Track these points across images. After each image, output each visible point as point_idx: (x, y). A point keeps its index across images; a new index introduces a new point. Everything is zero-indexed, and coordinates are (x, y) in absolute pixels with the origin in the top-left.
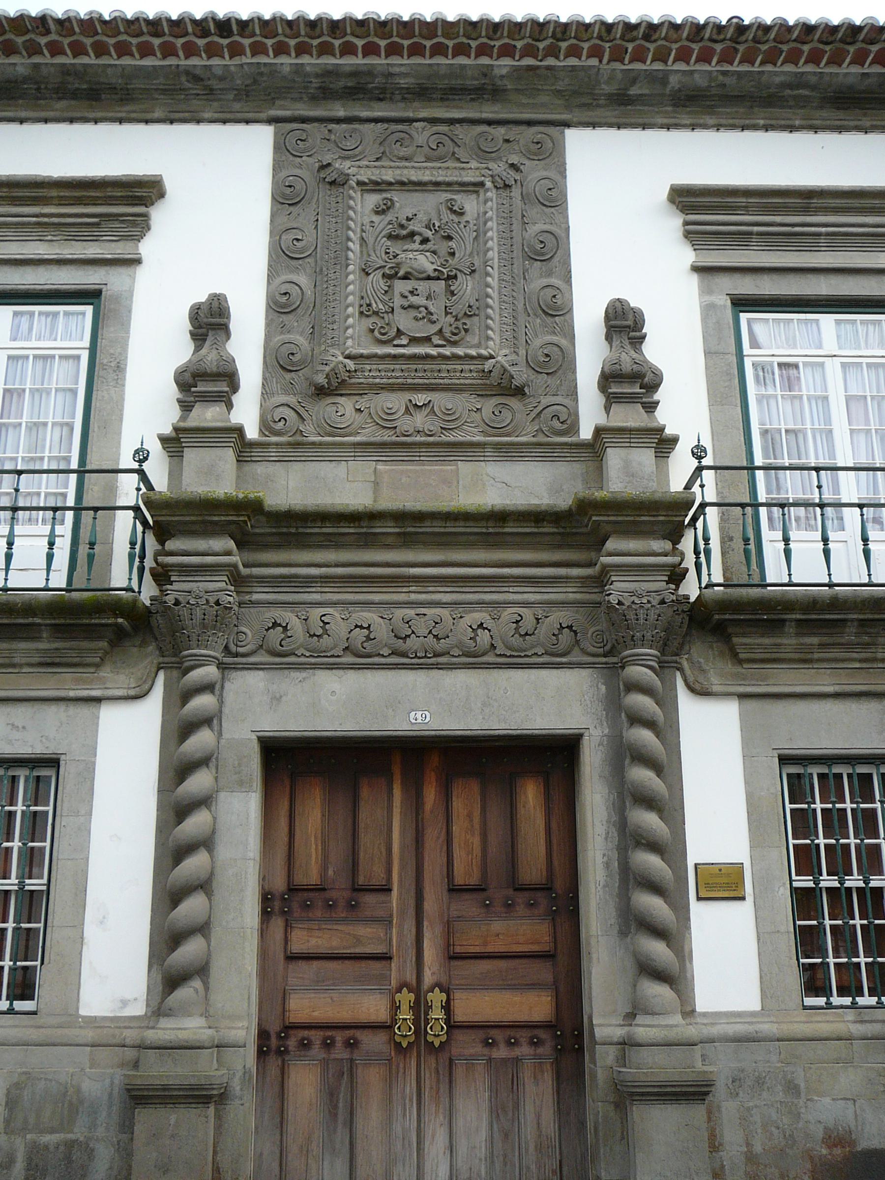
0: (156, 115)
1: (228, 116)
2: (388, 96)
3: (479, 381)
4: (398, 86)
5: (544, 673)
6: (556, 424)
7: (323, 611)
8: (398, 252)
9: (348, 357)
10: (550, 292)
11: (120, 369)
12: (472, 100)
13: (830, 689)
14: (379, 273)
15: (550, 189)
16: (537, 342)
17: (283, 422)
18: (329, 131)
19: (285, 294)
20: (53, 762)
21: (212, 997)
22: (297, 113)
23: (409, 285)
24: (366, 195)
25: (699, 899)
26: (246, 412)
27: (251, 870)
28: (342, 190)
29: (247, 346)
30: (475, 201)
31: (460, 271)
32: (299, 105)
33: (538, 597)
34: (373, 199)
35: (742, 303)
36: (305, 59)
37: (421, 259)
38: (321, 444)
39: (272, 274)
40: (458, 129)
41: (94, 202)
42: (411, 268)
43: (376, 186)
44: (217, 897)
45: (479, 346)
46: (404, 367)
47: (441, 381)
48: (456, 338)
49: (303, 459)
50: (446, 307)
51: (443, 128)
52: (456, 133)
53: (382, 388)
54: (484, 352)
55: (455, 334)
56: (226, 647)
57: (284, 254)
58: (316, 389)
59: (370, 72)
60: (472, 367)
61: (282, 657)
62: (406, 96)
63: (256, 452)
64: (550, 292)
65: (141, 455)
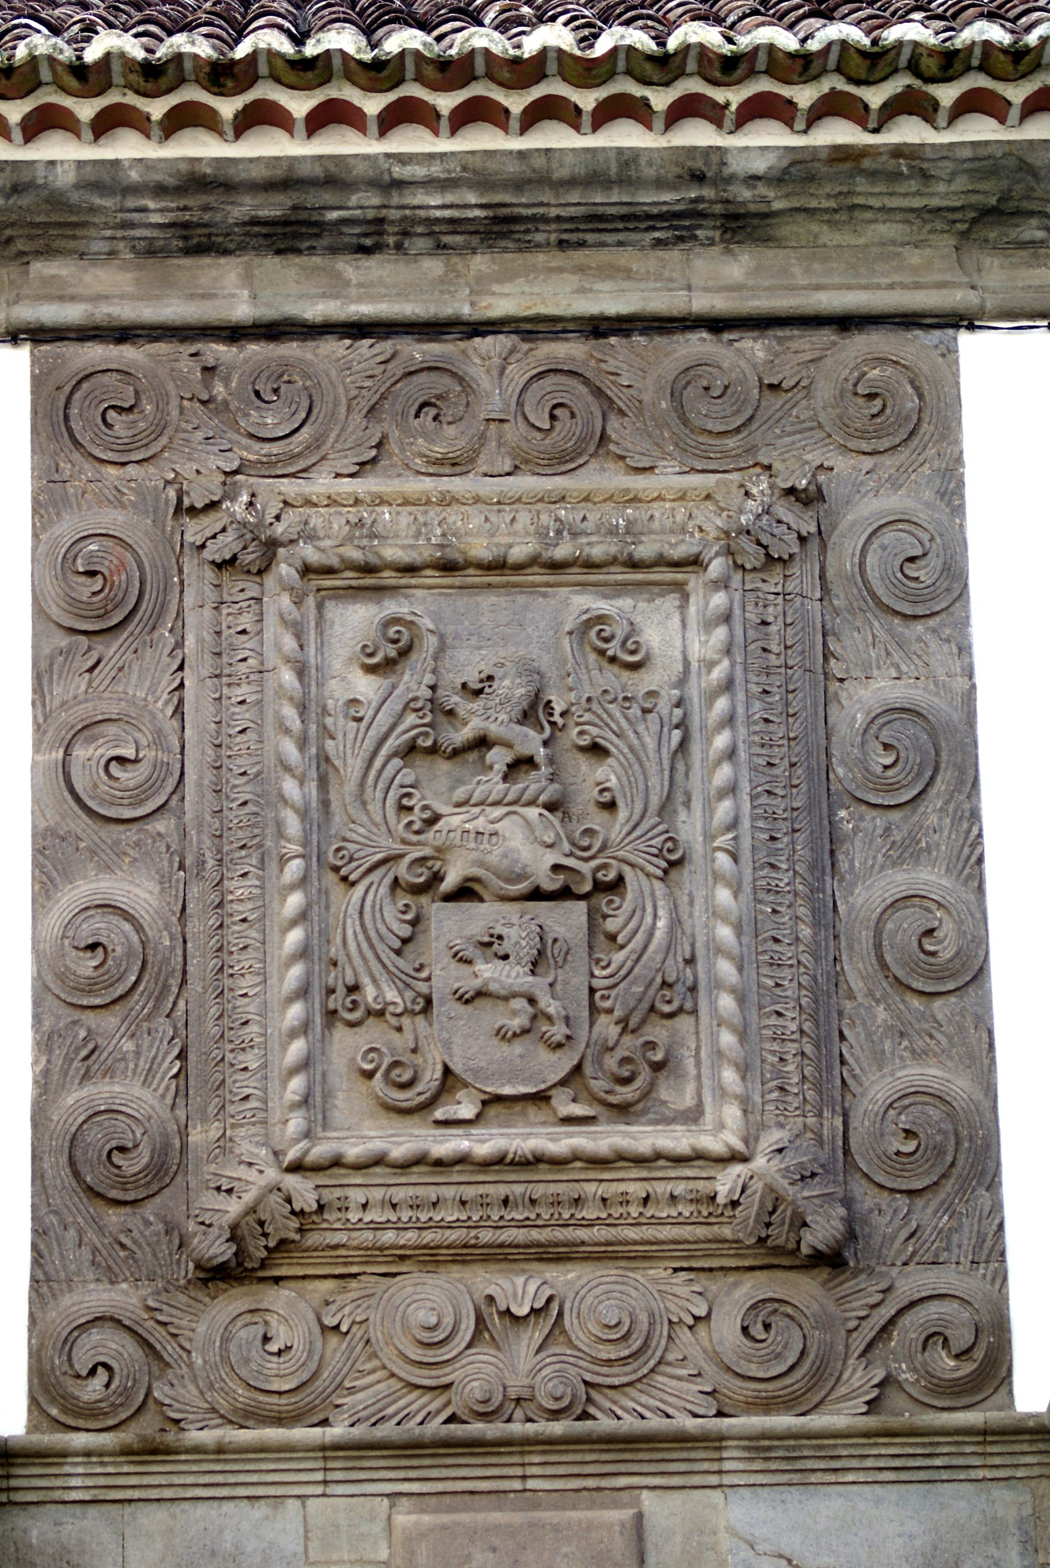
2: (391, 240)
3: (700, 1232)
4: (422, 213)
6: (946, 1364)
8: (443, 809)
9: (297, 1168)
10: (911, 921)
12: (658, 243)
14: (381, 879)
15: (912, 559)
17: (102, 1375)
18: (209, 370)
19: (93, 947)
24: (335, 611)
28: (253, 591)
30: (676, 621)
31: (632, 865)
39: (53, 860)
40: (620, 355)
42: (482, 864)
46: (470, 1192)
47: (582, 1234)
48: (626, 1093)
49: (168, 1493)
50: (592, 991)
51: (570, 350)
52: (612, 365)
53: (402, 1258)
54: (712, 1144)
55: (626, 1081)
58: (198, 1267)
59: (334, 177)
60: (680, 1188)
62: (446, 239)
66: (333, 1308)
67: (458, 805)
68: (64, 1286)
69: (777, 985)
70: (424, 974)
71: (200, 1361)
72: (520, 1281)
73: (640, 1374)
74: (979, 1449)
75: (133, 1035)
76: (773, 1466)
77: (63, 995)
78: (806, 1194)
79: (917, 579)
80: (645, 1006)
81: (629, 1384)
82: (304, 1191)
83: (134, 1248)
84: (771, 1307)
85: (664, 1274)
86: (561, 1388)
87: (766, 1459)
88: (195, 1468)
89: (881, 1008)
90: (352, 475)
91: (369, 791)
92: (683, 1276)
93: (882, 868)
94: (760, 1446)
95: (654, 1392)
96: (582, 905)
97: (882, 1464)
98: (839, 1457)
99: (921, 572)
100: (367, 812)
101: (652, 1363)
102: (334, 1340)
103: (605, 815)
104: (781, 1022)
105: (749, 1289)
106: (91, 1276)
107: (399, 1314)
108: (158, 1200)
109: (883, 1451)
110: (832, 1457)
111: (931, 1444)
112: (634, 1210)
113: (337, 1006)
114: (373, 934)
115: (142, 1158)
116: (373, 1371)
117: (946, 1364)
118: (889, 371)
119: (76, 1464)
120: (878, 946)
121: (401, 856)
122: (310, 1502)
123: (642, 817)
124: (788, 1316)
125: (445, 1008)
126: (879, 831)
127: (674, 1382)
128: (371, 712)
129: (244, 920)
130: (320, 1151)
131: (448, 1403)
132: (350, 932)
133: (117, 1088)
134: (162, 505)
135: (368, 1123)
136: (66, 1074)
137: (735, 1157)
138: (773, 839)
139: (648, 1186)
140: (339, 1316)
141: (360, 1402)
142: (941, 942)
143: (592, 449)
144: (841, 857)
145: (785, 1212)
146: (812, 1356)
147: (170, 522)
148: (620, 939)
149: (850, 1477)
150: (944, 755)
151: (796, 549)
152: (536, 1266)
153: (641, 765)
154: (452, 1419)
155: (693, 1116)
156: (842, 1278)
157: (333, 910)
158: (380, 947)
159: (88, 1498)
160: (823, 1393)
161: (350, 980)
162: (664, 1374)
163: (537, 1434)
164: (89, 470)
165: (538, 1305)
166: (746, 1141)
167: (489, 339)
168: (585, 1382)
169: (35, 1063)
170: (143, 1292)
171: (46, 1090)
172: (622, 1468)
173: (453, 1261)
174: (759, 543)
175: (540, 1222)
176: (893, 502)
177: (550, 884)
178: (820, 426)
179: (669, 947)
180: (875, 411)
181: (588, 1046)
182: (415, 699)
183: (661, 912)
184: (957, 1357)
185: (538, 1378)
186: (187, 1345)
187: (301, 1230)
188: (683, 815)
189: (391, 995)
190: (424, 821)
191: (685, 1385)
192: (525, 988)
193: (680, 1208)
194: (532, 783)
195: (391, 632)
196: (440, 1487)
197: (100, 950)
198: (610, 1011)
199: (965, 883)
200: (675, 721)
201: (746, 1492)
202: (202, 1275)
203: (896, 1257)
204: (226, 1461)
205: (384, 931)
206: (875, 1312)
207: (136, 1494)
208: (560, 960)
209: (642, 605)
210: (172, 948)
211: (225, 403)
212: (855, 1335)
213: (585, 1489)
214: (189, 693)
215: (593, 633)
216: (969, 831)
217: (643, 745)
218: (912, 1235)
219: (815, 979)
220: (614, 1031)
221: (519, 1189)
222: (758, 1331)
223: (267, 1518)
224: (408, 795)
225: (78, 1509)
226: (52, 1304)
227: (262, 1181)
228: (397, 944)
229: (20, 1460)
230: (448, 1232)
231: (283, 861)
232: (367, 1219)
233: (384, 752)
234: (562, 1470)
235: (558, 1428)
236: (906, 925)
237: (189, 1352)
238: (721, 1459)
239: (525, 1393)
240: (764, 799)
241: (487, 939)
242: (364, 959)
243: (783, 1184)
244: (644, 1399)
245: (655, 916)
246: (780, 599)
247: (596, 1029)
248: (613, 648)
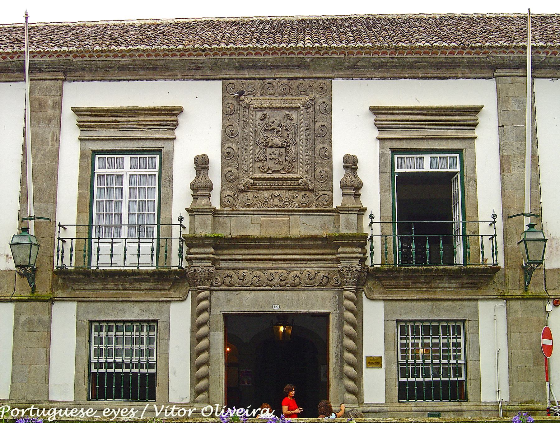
0: (178, 77)
1: (205, 77)
5: (318, 292)
6: (325, 202)
7: (244, 271)
11: (171, 181)
13: (415, 298)
16: (319, 170)
20: (156, 322)
21: (210, 397)
22: (231, 76)
23: (272, 150)
25: (367, 367)
26: (216, 202)
27: (221, 357)
29: (215, 175)
32: (230, 72)
33: (316, 265)
34: (259, 114)
35: (394, 152)
36: (233, 57)
37: (277, 139)
38: (242, 211)
39: (223, 143)
40: (292, 82)
41: (158, 115)
43: (261, 109)
44: (211, 366)
45: (297, 173)
48: (289, 170)
54: (299, 177)
56: (211, 284)
57: (227, 136)
61: (231, 287)
63: (220, 213)
64: (323, 150)
65: (181, 219)
105: (303, 193)
113: (257, 160)
130: (254, 177)
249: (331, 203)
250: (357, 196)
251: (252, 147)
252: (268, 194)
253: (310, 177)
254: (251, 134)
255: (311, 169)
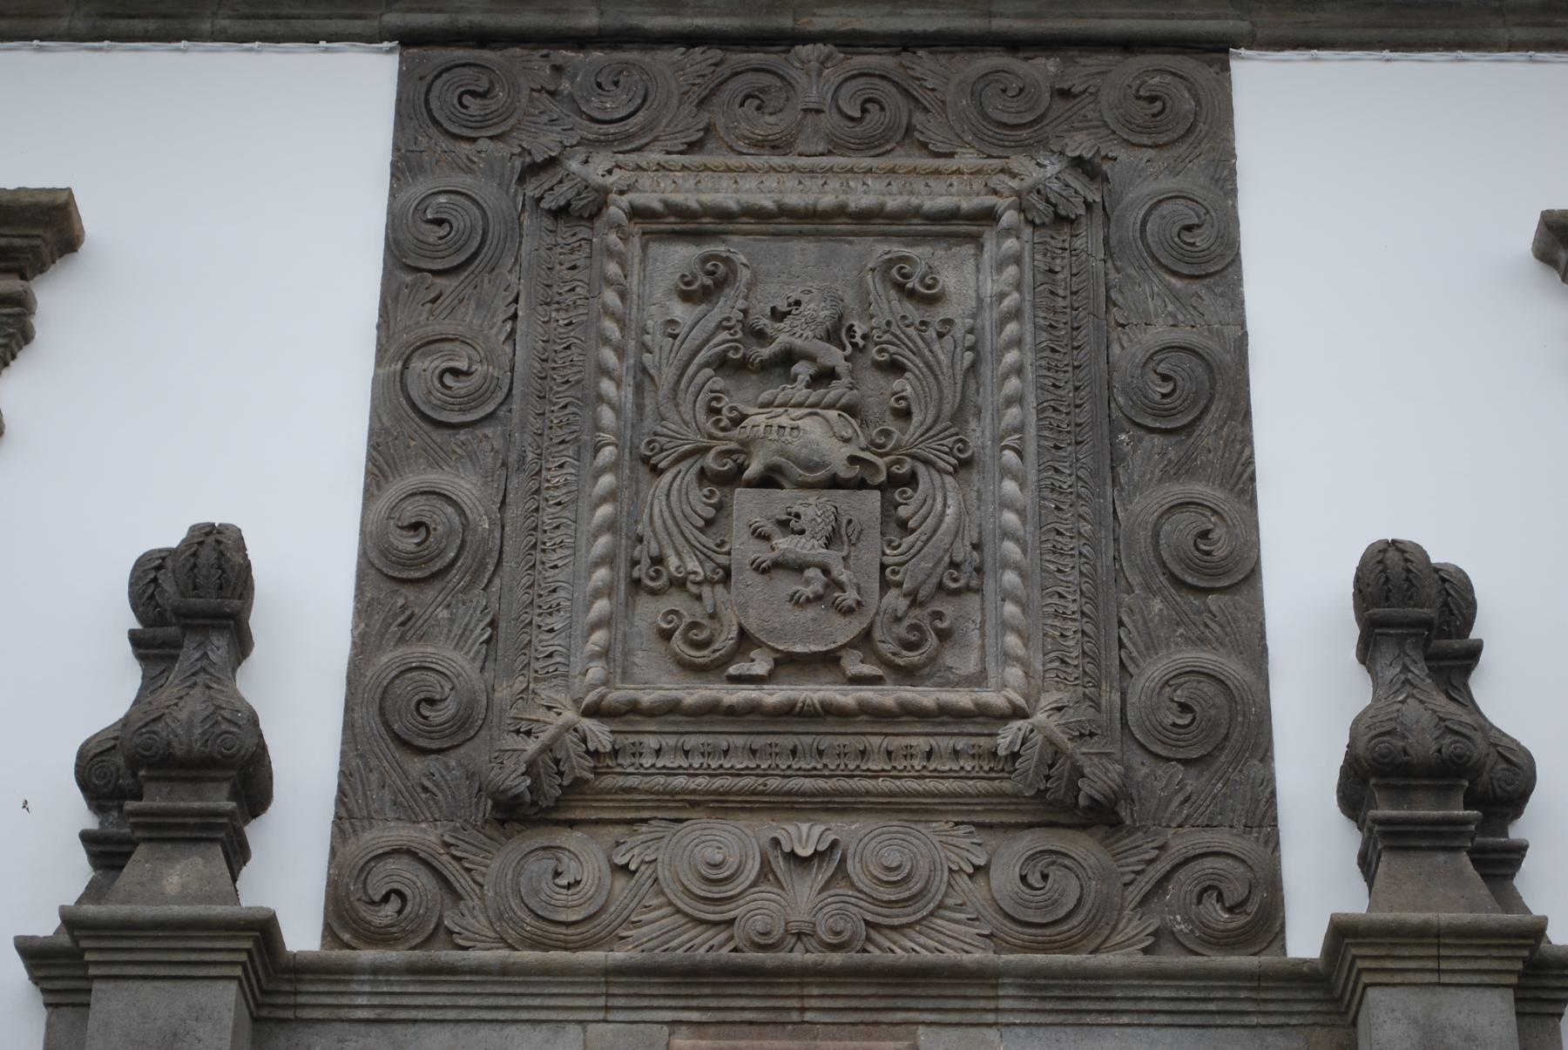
3: (982, 785)
6: (1219, 916)
8: (751, 410)
9: (594, 711)
14: (689, 470)
15: (1189, 228)
16: (1153, 671)
18: (557, 69)
23: (782, 499)
24: (656, 249)
29: (299, 684)
30: (971, 265)
34: (682, 256)
39: (383, 461)
40: (925, 63)
43: (686, 224)
46: (759, 742)
47: (868, 784)
48: (913, 657)
49: (451, 1015)
50: (883, 567)
52: (918, 72)
54: (993, 698)
57: (416, 416)
60: (961, 743)
66: (623, 848)
67: (763, 406)
68: (366, 823)
69: (1059, 571)
70: (725, 549)
71: (491, 894)
72: (805, 827)
73: (919, 915)
74: (1253, 995)
75: (448, 606)
76: (1050, 1006)
77: (385, 570)
78: (1084, 750)
79: (1193, 244)
80: (934, 580)
81: (909, 925)
82: (600, 734)
83: (435, 790)
84: (1048, 859)
85: (946, 827)
86: (842, 923)
87: (1043, 998)
88: (479, 990)
89: (1158, 600)
90: (681, 153)
91: (681, 394)
92: (963, 829)
93: (1160, 480)
94: (1036, 983)
95: (933, 933)
96: (877, 494)
97: (1156, 1006)
98: (1113, 999)
99: (1200, 240)
100: (679, 413)
101: (931, 906)
102: (621, 882)
103: (901, 424)
104: (1062, 602)
105: (1028, 842)
106: (390, 815)
107: (687, 853)
108: (462, 750)
109: (1157, 994)
110: (1107, 999)
111: (1205, 988)
112: (917, 764)
113: (642, 579)
114: (678, 513)
115: (447, 710)
116: (660, 907)
117: (1219, 916)
118: (1168, 79)
119: (363, 982)
120: (1156, 544)
121: (709, 449)
122: (590, 1027)
123: (935, 422)
124: (1066, 867)
125: (744, 578)
126: (1157, 450)
127: (953, 926)
128: (686, 329)
129: (559, 504)
130: (618, 695)
131: (731, 938)
132: (656, 511)
133: (429, 650)
134: (507, 173)
135: (664, 679)
136: (383, 636)
137: (1018, 713)
138: (1057, 447)
139: (932, 741)
140: (628, 856)
141: (644, 935)
142: (1215, 543)
143: (898, 137)
144: (1120, 470)
145: (1063, 767)
146: (1088, 905)
147: (513, 186)
148: (911, 524)
149: (1125, 1019)
150: (1218, 386)
151: (1082, 211)
152: (824, 816)
153: (936, 377)
154: (735, 950)
155: (978, 680)
156: (1119, 835)
157: (642, 495)
158: (684, 524)
159: (372, 1016)
160: (1099, 940)
161: (654, 550)
162: (942, 918)
163: (816, 964)
164: (445, 143)
165: (821, 848)
166: (1026, 697)
167: (810, 47)
168: (867, 923)
169: (355, 627)
170: (439, 831)
171: (363, 649)
172: (899, 1003)
173: (742, 809)
174: (1048, 201)
175: (826, 773)
176: (1169, 184)
177: (845, 472)
178: (1106, 125)
179: (957, 533)
180: (1155, 111)
181: (877, 613)
182: (728, 319)
183: (950, 502)
184: (1230, 910)
185: (820, 915)
186: (480, 880)
187: (594, 770)
188: (973, 424)
189: (693, 565)
190: (731, 420)
191: (963, 928)
192: (819, 558)
193: (962, 763)
194: (835, 391)
195: (709, 266)
196: (720, 1016)
197: (423, 531)
198: (899, 585)
199: (1238, 496)
200: (967, 344)
201: (1022, 1031)
202: (498, 816)
203: (1171, 820)
204: (509, 983)
205: (688, 511)
206: (1150, 868)
207: (421, 1015)
208: (854, 538)
209: (940, 253)
210: (491, 531)
211: (571, 96)
212: (1131, 888)
213: (862, 1023)
214: (521, 326)
215: (894, 271)
216: (1242, 452)
217: (939, 362)
218: (1187, 799)
219: (1094, 567)
220: (903, 604)
221: (807, 740)
222: (1034, 879)
223: (547, 1041)
224: (718, 399)
225: (362, 1028)
226: (353, 839)
227: (560, 721)
228: (701, 523)
229: (308, 977)
230: (737, 780)
231: (597, 449)
232: (659, 765)
233: (697, 361)
234: (839, 1003)
235: (837, 958)
236: (1182, 527)
237: (481, 886)
238: (997, 997)
239: (807, 929)
240: (1049, 413)
241: (785, 517)
242: (669, 534)
243: (1062, 737)
244: (922, 940)
245: (945, 505)
246: (1067, 254)
247: (885, 600)
248: (912, 283)
249: (1267, 921)
250: (1500, 863)
251: (607, 480)
252: (732, 842)
253: (1085, 713)
254: (607, 386)
255: (1098, 657)
